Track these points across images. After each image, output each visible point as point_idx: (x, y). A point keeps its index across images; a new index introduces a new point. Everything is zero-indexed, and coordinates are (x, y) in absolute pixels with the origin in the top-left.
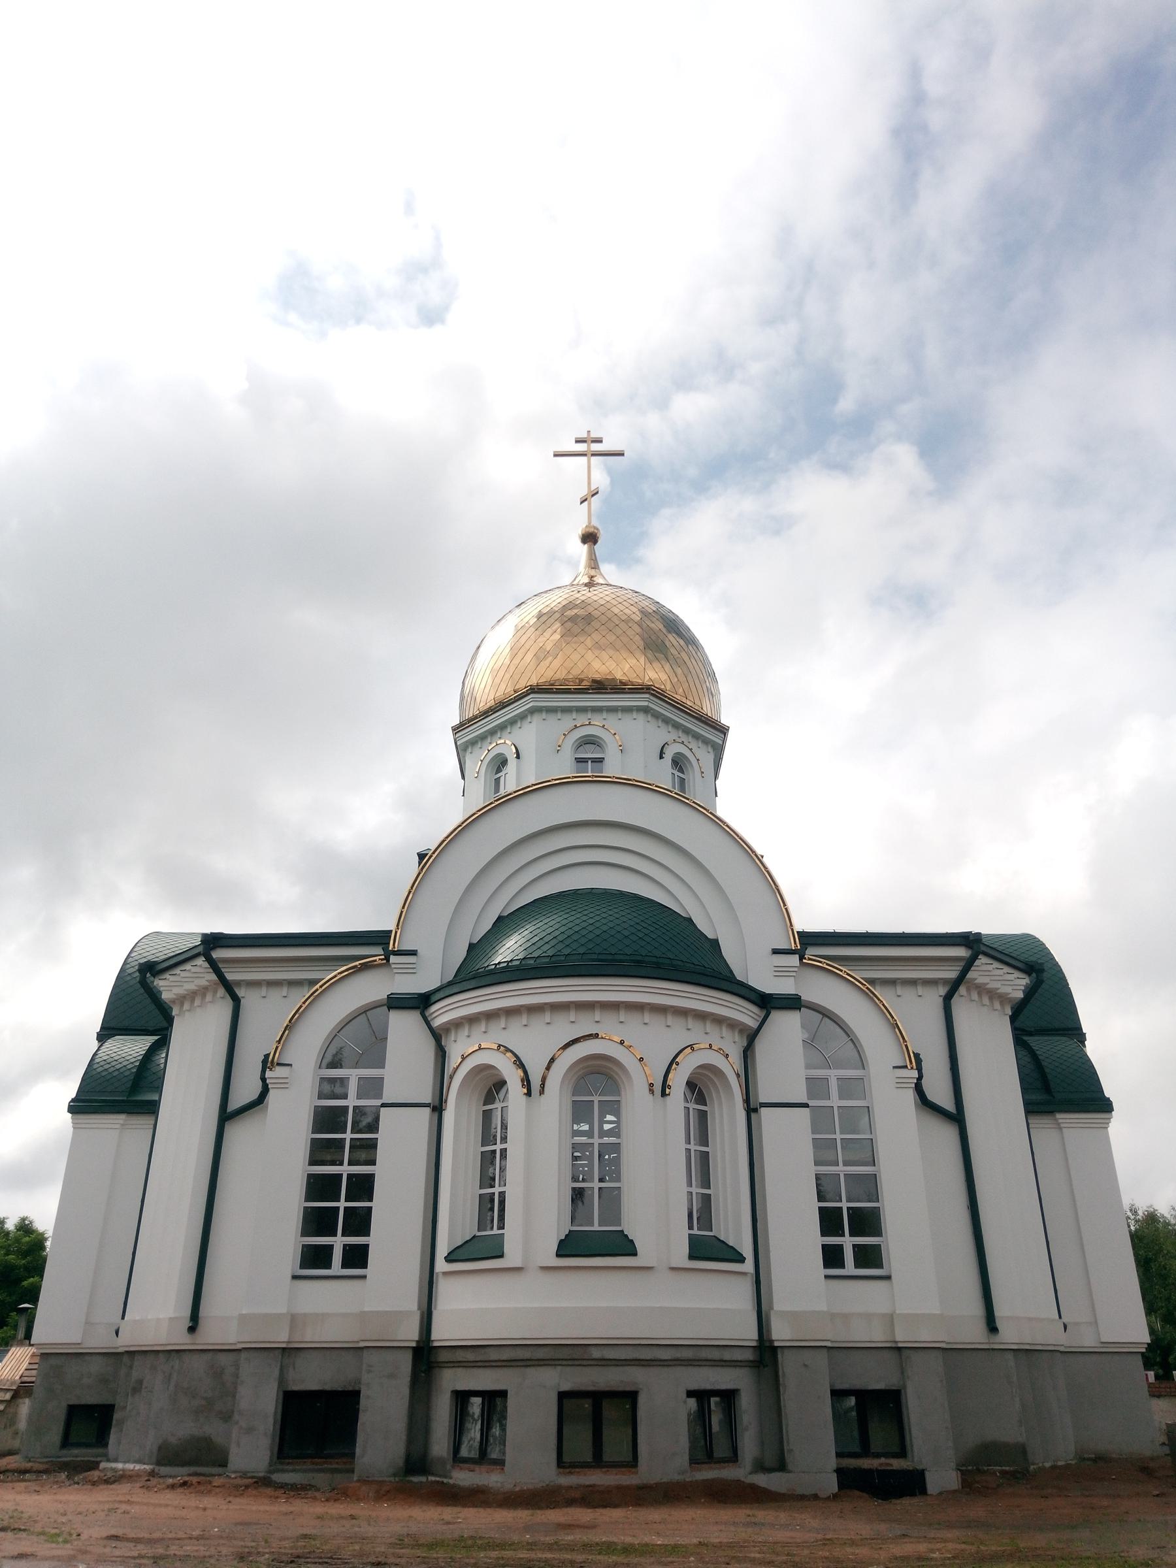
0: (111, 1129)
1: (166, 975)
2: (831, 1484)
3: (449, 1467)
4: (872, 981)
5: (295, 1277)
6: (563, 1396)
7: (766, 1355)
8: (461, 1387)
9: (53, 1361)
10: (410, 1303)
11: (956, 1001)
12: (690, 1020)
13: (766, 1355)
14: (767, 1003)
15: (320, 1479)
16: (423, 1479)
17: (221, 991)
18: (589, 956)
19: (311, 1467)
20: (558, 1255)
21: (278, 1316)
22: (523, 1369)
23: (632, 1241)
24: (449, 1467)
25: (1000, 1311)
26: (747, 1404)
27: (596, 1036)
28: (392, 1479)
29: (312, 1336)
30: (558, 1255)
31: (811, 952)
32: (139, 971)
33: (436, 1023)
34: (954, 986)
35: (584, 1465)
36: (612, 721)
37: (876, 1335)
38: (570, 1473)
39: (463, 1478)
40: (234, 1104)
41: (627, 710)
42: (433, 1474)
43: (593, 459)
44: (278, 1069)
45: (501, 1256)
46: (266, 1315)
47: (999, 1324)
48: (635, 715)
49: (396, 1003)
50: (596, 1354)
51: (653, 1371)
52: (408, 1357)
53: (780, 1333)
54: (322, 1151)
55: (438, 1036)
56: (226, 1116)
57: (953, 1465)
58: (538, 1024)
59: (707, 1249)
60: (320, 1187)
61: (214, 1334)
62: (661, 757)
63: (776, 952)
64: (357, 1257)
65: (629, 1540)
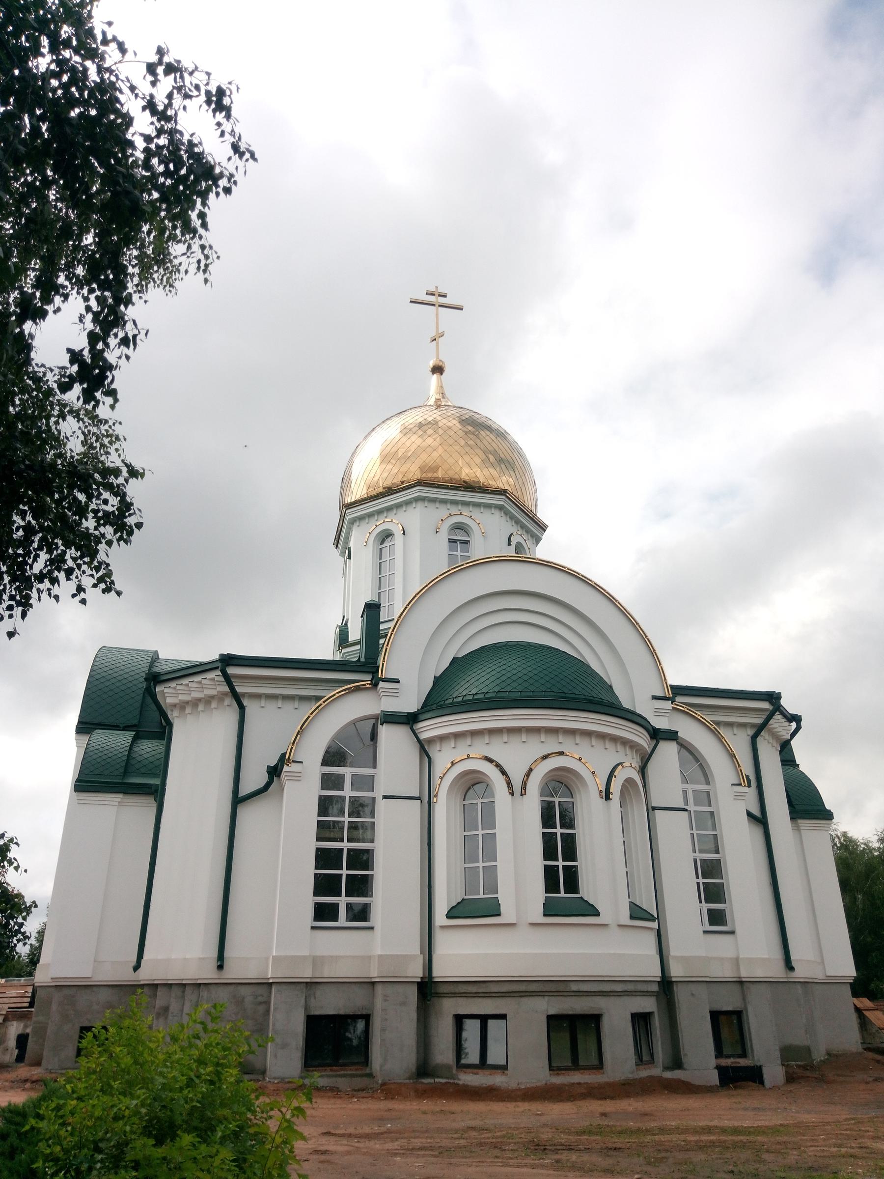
0: (108, 808)
1: (173, 684)
2: (714, 1078)
3: (454, 1071)
4: (718, 723)
5: (313, 928)
6: (550, 1018)
7: (666, 986)
8: (462, 1011)
9: (66, 992)
10: (413, 947)
11: (759, 740)
12: (607, 742)
13: (666, 986)
14: (657, 735)
15: (342, 1083)
16: (431, 1080)
17: (229, 701)
18: (549, 694)
19: (331, 1073)
20: (545, 915)
21: (305, 957)
22: (517, 999)
23: (592, 905)
24: (454, 1071)
25: (793, 957)
26: (656, 1021)
27: (561, 753)
28: (408, 1081)
29: (329, 972)
30: (545, 915)
31: (679, 699)
32: (146, 679)
33: (423, 736)
34: (759, 729)
35: (567, 1069)
36: (476, 513)
37: (726, 973)
38: (558, 1074)
39: (468, 1079)
40: (244, 791)
41: (488, 506)
42: (438, 1077)
43: (440, 308)
44: (293, 764)
45: (499, 915)
46: (292, 957)
47: (794, 964)
48: (493, 510)
49: (390, 718)
50: (574, 987)
51: (612, 1000)
52: (415, 989)
53: (676, 971)
54: (325, 830)
55: (424, 748)
56: (238, 800)
57: (779, 1062)
58: (515, 742)
59: (637, 913)
60: (325, 858)
61: (235, 971)
62: (509, 544)
63: (655, 698)
64: (361, 914)
65: (736, 1124)
